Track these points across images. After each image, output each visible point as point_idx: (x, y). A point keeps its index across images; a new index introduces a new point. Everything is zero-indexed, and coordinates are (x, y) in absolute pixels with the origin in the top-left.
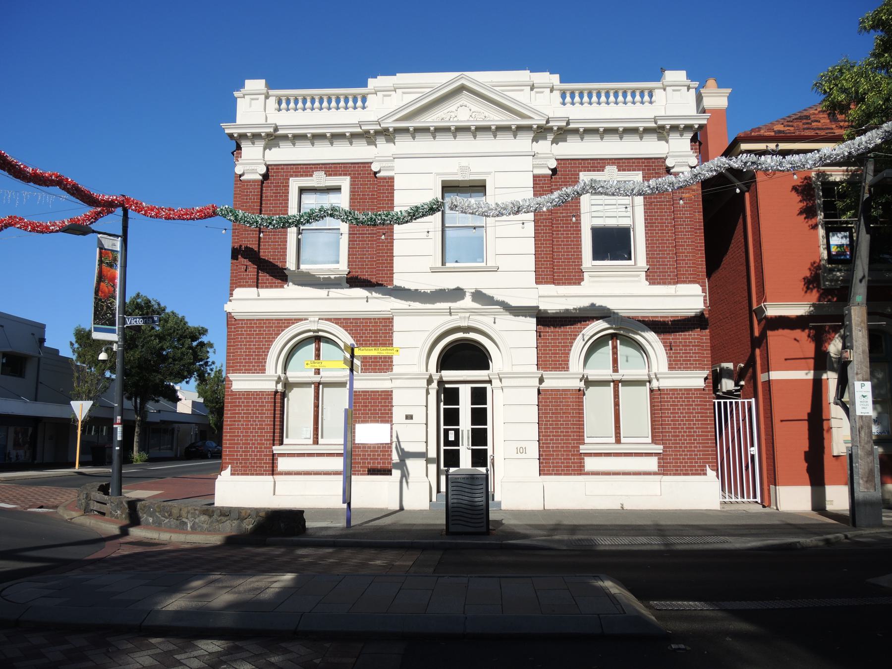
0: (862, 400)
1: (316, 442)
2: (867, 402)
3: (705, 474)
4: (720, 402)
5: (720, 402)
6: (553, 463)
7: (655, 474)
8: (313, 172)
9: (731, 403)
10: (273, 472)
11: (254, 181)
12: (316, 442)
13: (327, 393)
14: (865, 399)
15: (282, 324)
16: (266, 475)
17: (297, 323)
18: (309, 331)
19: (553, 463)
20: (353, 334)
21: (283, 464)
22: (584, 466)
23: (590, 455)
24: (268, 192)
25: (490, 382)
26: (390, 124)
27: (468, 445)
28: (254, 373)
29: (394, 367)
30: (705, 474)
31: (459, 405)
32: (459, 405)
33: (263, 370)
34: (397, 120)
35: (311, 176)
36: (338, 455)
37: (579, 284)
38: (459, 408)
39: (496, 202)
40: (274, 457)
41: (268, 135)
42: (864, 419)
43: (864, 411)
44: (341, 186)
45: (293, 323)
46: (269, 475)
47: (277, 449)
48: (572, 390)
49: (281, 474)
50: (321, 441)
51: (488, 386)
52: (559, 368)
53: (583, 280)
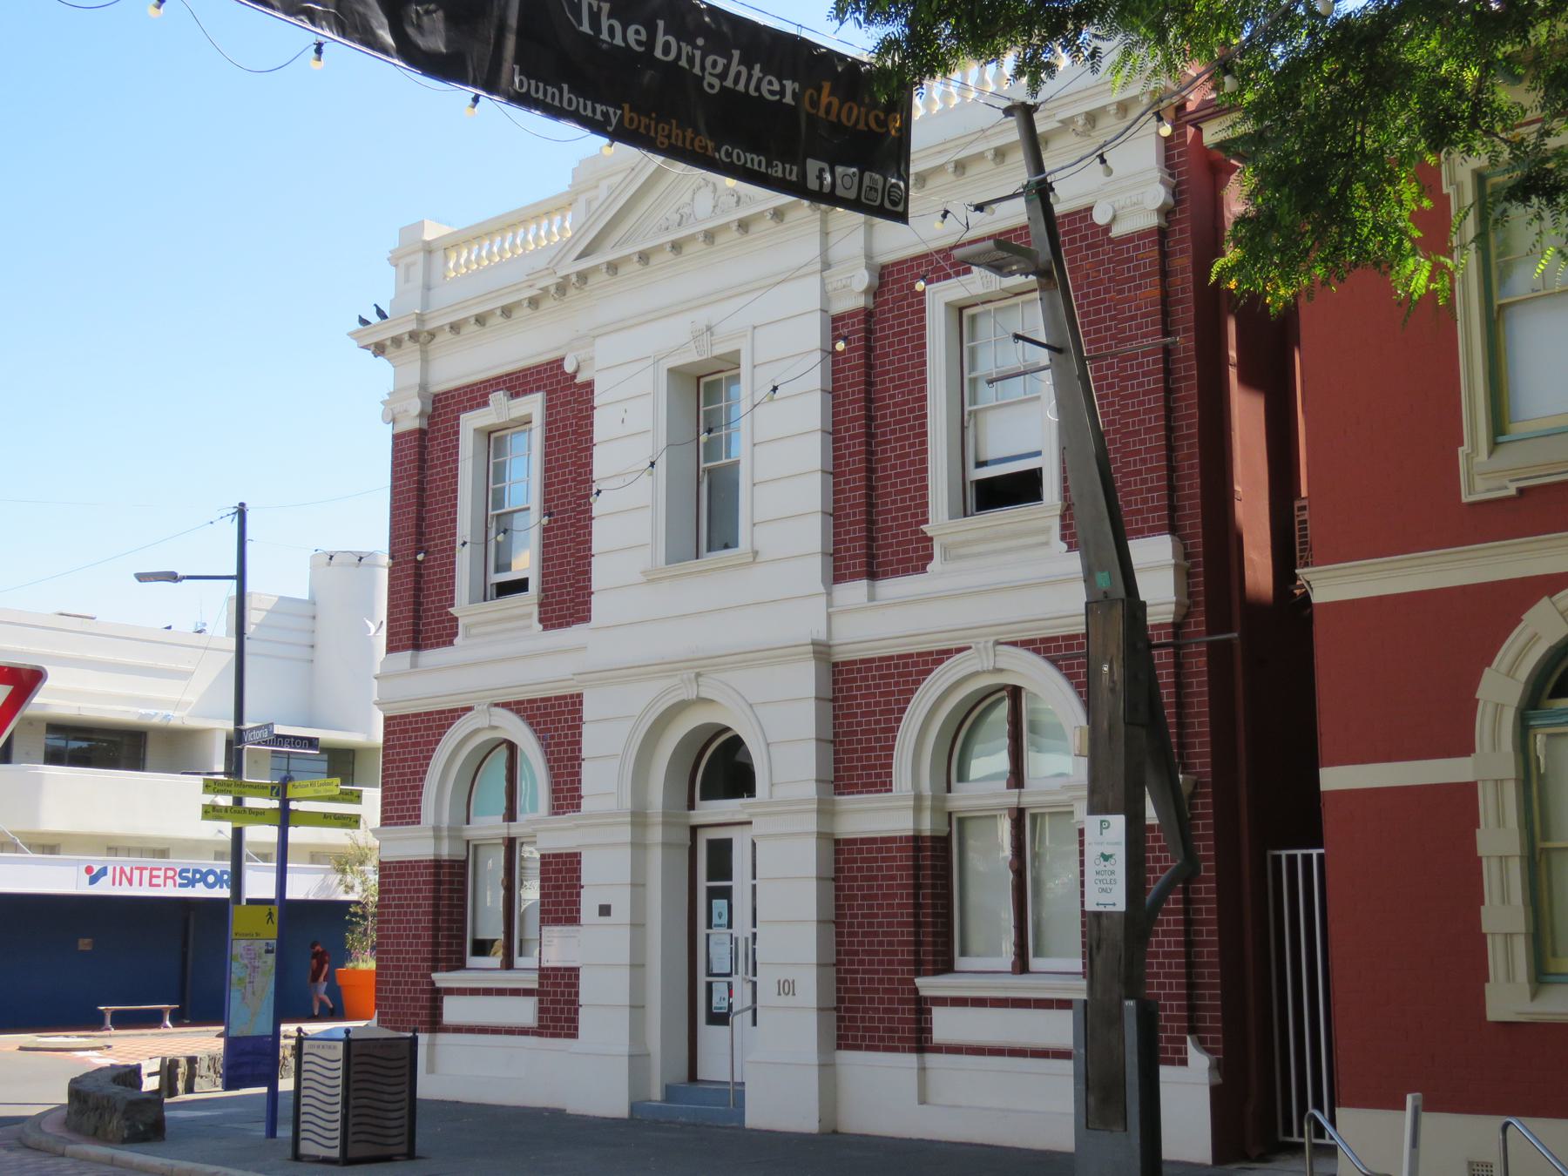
0: (1101, 868)
1: (1021, 965)
2: (1113, 873)
5: (1310, 856)
6: (863, 1019)
7: (524, 1032)
8: (486, 395)
9: (1307, 859)
10: (921, 1041)
11: (1142, 235)
12: (1021, 965)
13: (144, 872)
14: (1109, 866)
15: (915, 666)
16: (904, 1051)
17: (948, 658)
18: (976, 674)
20: (541, 731)
21: (946, 1025)
22: (930, 1031)
23: (942, 1001)
24: (435, 452)
25: (694, 830)
26: (571, 267)
27: (747, 973)
28: (880, 791)
34: (580, 257)
35: (486, 404)
36: (528, 992)
41: (413, 336)
42: (1105, 922)
43: (1105, 898)
44: (948, 305)
45: (940, 662)
46: (911, 1050)
47: (928, 985)
49: (939, 1049)
50: (1035, 963)
53: (930, 557)
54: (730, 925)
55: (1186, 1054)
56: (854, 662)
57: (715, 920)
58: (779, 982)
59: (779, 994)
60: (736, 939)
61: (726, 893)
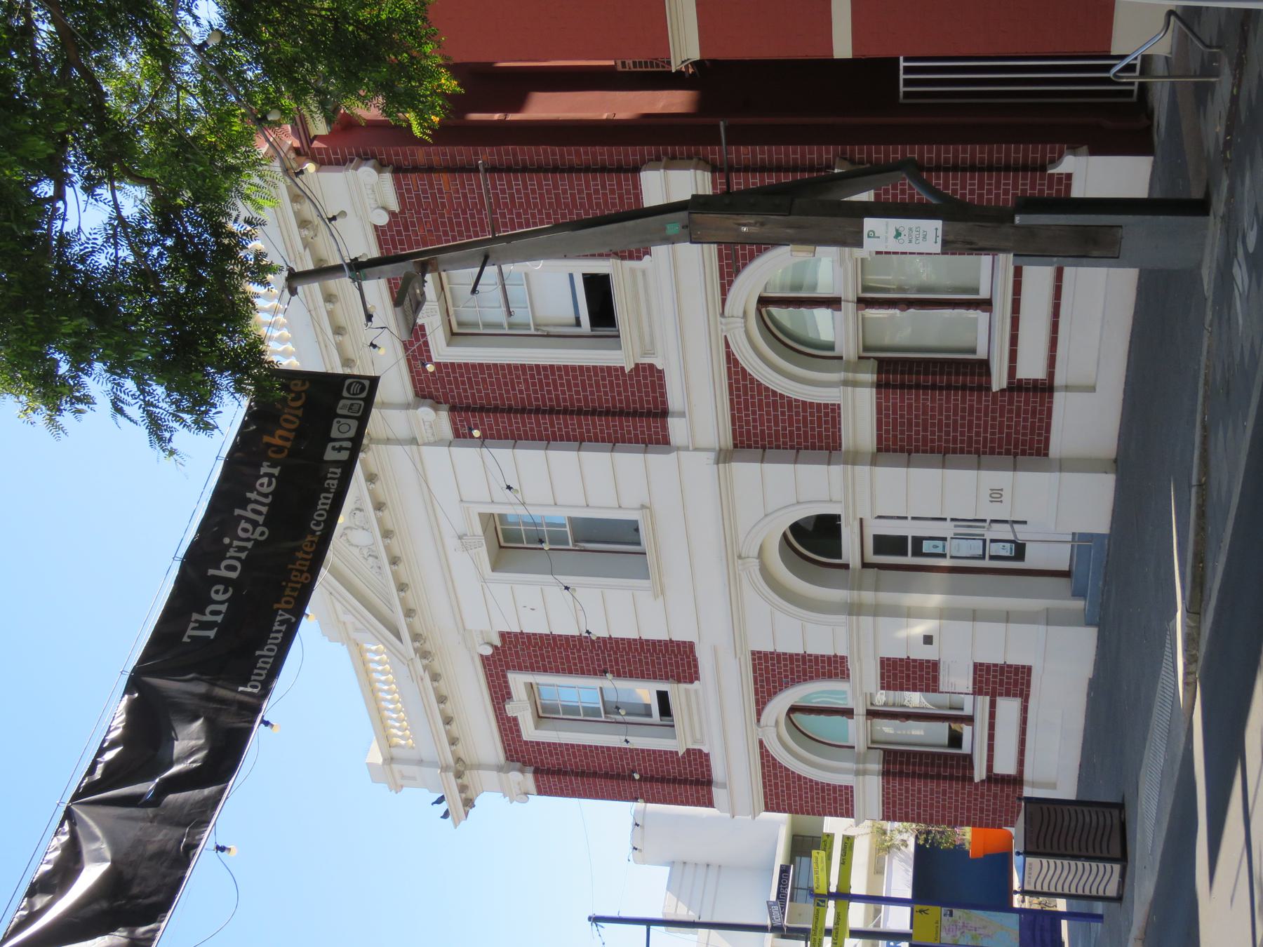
2: (910, 229)
3: (1069, 176)
4: (905, 80)
5: (905, 80)
6: (1024, 435)
7: (1025, 710)
8: (508, 718)
10: (1044, 389)
17: (733, 355)
19: (1024, 435)
20: (781, 685)
21: (1031, 368)
22: (1036, 381)
26: (408, 647)
28: (839, 414)
29: (840, 653)
30: (1069, 176)
31: (907, 537)
32: (907, 537)
33: (849, 789)
35: (515, 719)
36: (993, 705)
37: (707, 755)
38: (913, 537)
39: (470, 296)
40: (1016, 386)
41: (459, 775)
46: (1051, 397)
47: (999, 381)
48: (877, 398)
49: (1051, 374)
50: (984, 294)
51: (870, 746)
52: (834, 418)
54: (944, 539)
55: (1062, 174)
56: (734, 431)
57: (939, 551)
58: (991, 501)
59: (1001, 501)
60: (955, 534)
61: (918, 541)
